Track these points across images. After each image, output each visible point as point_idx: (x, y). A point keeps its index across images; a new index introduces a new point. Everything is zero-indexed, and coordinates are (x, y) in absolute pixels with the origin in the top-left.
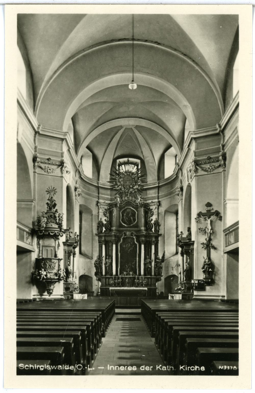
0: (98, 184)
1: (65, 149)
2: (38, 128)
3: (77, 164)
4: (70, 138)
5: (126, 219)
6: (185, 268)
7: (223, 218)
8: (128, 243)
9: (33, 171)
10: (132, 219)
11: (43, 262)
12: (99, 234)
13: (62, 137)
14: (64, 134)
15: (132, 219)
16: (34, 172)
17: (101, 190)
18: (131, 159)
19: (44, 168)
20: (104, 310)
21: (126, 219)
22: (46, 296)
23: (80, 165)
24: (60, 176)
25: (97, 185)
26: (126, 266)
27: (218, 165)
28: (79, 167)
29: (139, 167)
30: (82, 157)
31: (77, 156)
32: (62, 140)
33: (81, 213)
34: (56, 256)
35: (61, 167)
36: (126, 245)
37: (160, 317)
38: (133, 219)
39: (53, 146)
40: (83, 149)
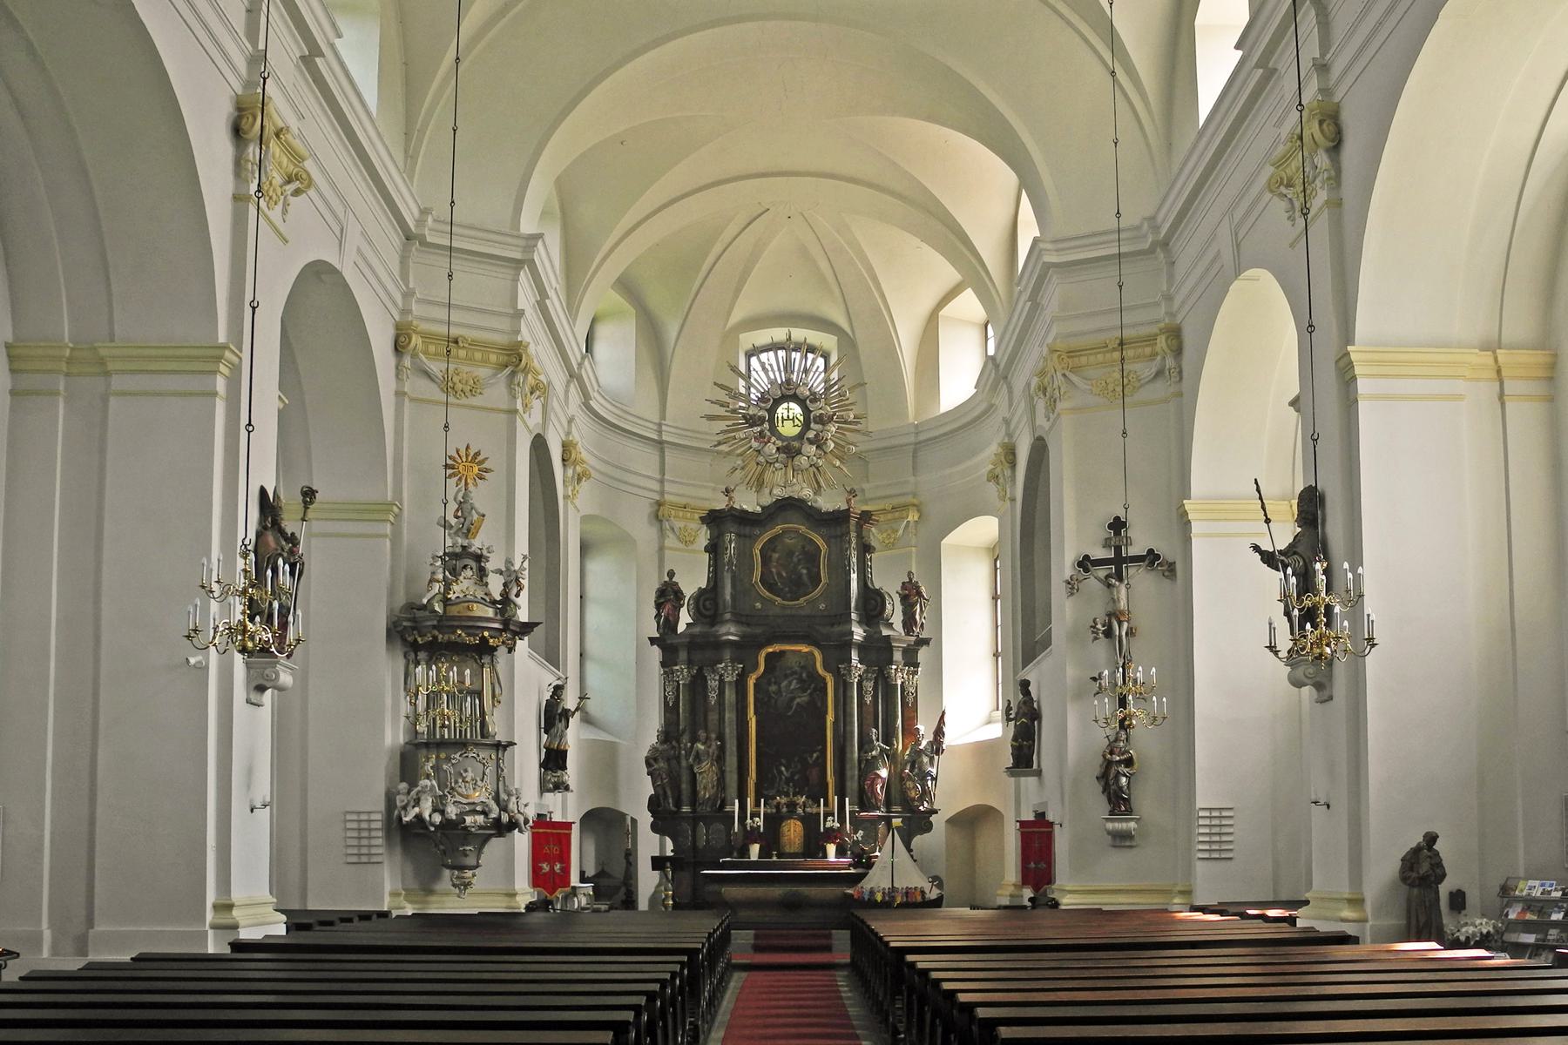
0: (660, 432)
1: (526, 299)
2: (420, 222)
4: (549, 257)
5: (779, 574)
6: (922, 961)
7: (1179, 567)
8: (786, 676)
9: (393, 385)
10: (805, 578)
11: (192, 661)
12: (666, 640)
13: (518, 256)
14: (522, 242)
15: (805, 578)
16: (400, 394)
17: (670, 455)
18: (799, 334)
19: (440, 375)
20: (697, 951)
21: (779, 574)
22: (449, 903)
23: (583, 358)
24: (505, 407)
25: (655, 437)
26: (781, 773)
27: (1154, 370)
28: (580, 365)
29: (834, 359)
30: (594, 321)
32: (517, 264)
33: (585, 548)
34: (484, 733)
35: (508, 371)
36: (778, 683)
37: (926, 972)
38: (809, 573)
39: (476, 285)
40: (600, 294)
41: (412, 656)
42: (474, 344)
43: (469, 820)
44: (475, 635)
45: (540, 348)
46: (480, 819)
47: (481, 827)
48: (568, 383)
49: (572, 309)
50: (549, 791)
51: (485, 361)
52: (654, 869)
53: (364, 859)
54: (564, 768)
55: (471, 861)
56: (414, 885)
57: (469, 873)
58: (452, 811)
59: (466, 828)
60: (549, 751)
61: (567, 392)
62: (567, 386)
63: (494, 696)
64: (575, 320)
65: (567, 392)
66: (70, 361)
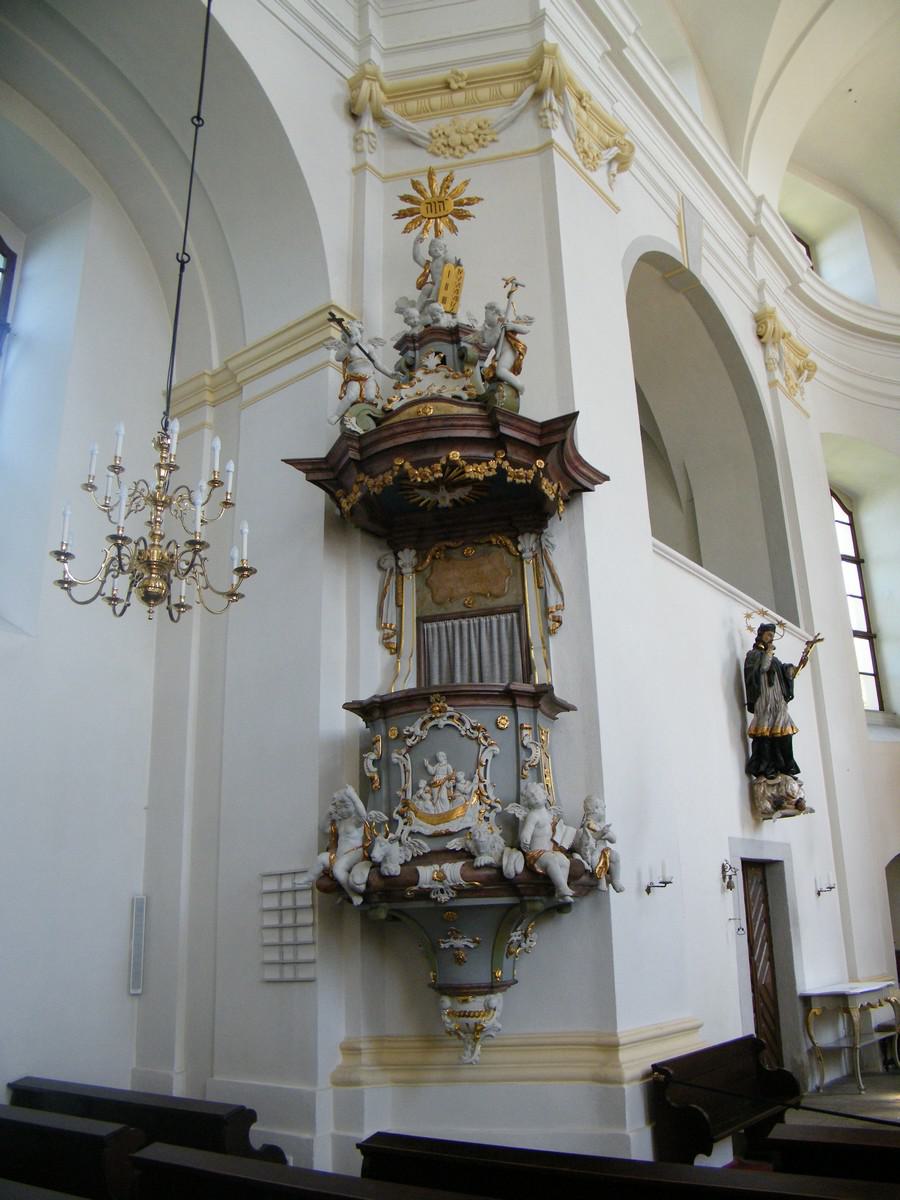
3: (747, 205)
28: (757, 214)
31: (747, 178)
41: (390, 562)
42: (473, 81)
43: (426, 874)
44: (430, 463)
45: (617, 106)
46: (453, 870)
47: (461, 892)
48: (750, 245)
49: (738, 165)
50: (768, 815)
51: (498, 99)
52: (653, 1066)
53: (289, 974)
54: (791, 769)
55: (476, 972)
56: (398, 1021)
57: (476, 1004)
58: (393, 856)
59: (424, 894)
60: (759, 741)
61: (750, 258)
62: (750, 251)
63: (546, 611)
64: (746, 172)
65: (750, 258)
66: (214, 389)
